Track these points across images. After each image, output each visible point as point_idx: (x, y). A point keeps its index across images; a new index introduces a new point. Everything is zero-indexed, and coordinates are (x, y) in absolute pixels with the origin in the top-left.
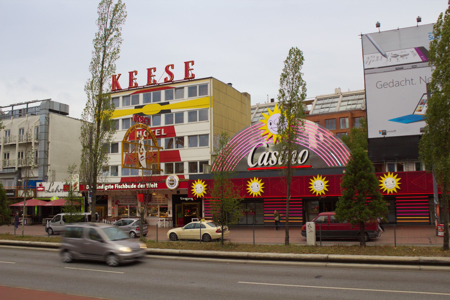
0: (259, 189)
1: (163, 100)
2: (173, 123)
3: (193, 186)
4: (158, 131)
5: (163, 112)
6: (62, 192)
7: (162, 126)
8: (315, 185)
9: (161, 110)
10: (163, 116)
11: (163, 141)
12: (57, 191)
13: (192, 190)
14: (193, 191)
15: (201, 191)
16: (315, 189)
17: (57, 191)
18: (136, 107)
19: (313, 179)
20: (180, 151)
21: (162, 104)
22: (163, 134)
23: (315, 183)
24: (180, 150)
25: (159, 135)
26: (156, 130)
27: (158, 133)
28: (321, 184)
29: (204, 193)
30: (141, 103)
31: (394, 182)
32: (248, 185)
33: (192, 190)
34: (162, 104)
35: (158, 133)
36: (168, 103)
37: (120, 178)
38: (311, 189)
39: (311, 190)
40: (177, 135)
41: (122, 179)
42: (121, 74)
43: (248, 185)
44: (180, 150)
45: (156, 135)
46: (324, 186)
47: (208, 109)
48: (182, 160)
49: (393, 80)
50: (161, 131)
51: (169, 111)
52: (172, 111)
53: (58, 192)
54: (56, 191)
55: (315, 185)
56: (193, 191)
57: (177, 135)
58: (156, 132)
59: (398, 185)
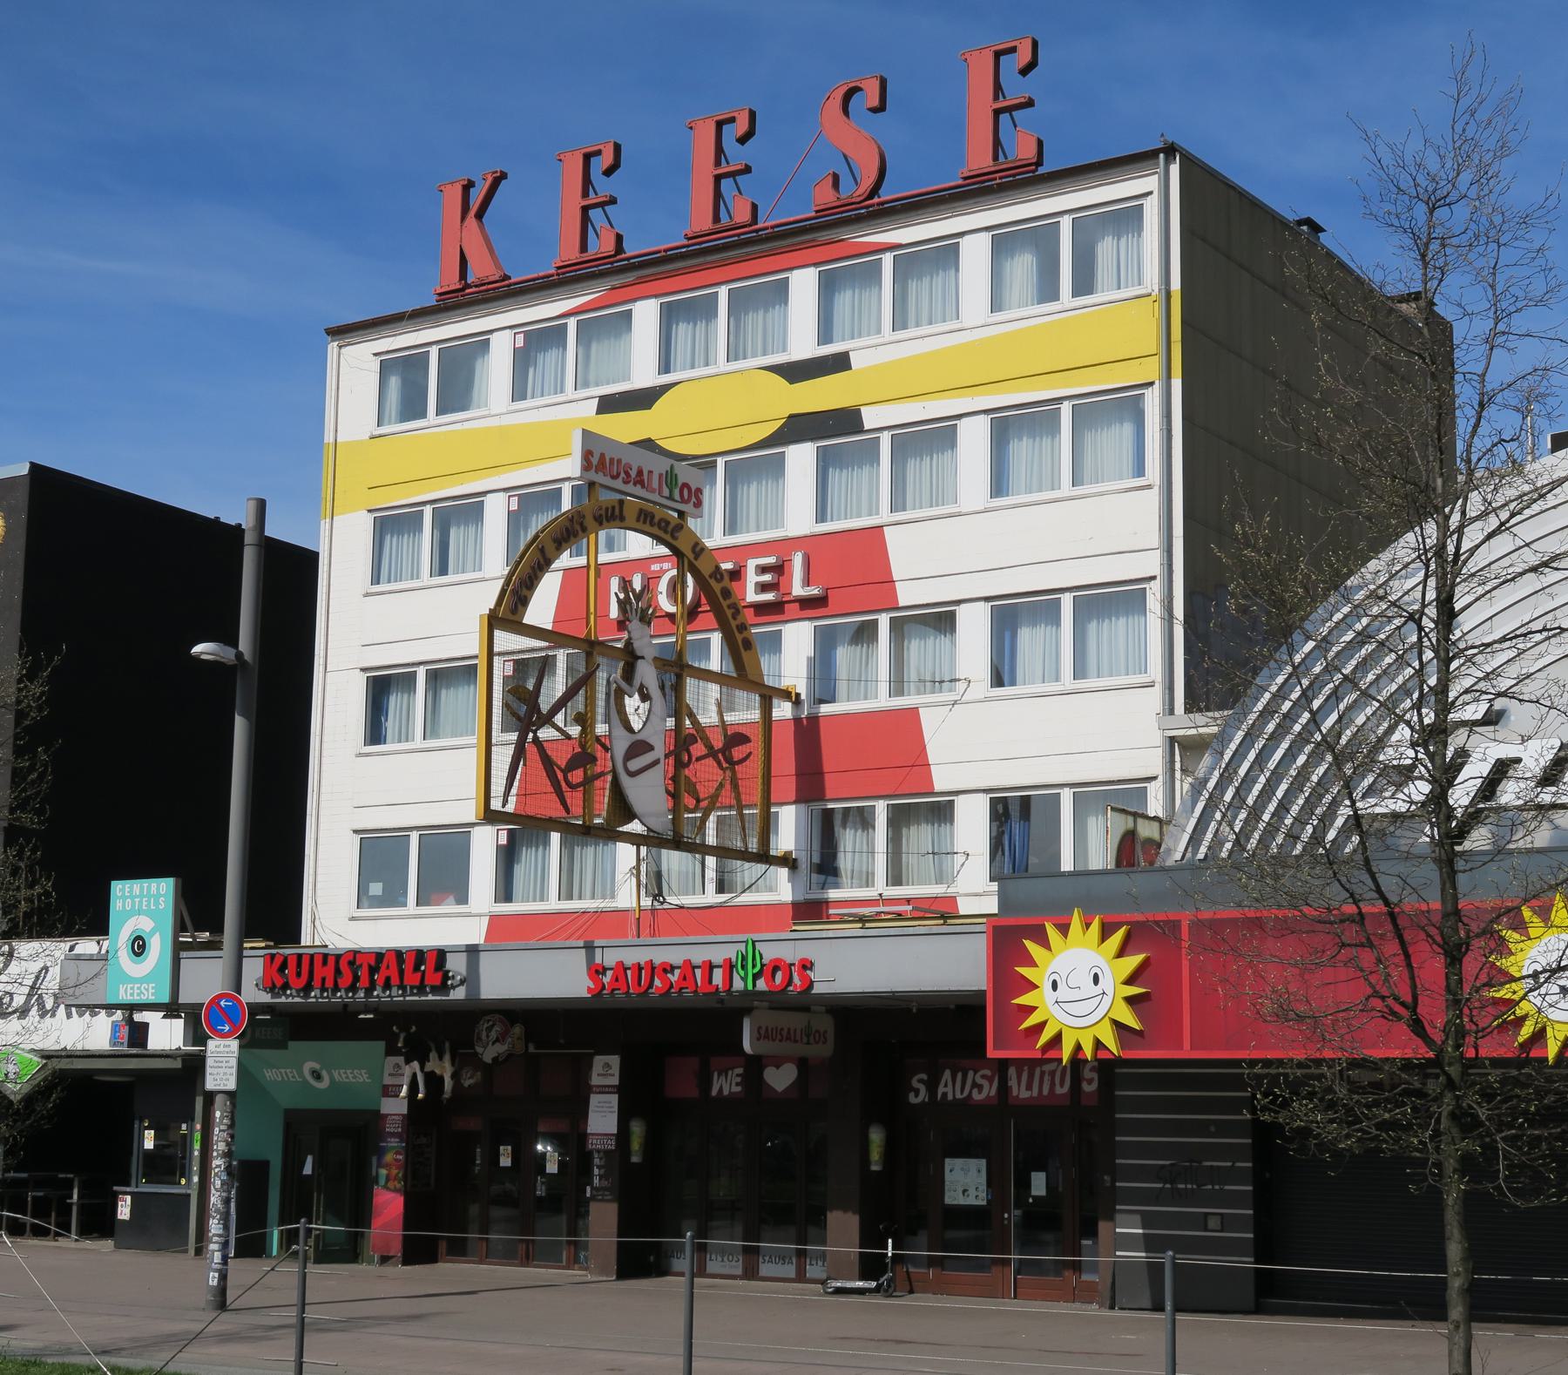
0: (1107, 1001)
1: (803, 345)
2: (873, 510)
3: (1031, 963)
4: (763, 570)
5: (798, 428)
6: (69, 1016)
7: (791, 534)
8: (1055, 986)
9: (791, 417)
10: (801, 458)
11: (798, 639)
12: (34, 1011)
13: (1024, 1000)
14: (1033, 1009)
15: (1091, 1005)
16: (1056, 1010)
17: (34, 1011)
18: (608, 405)
19: (1045, 943)
20: (924, 714)
21: (795, 372)
22: (798, 590)
23: (1053, 967)
24: (927, 705)
25: (769, 597)
26: (752, 564)
27: (763, 588)
28: (1096, 980)
29: (1118, 1026)
30: (644, 375)
31: (1107, 983)
32: (1024, 971)
33: (1024, 1000)
34: (795, 372)
35: (763, 588)
36: (840, 363)
37: (485, 921)
38: (1031, 1010)
39: (1031, 1021)
40: (907, 595)
41: (496, 921)
42: (503, 176)
43: (1024, 971)
44: (927, 705)
45: (752, 596)
46: (1110, 992)
47: (1148, 392)
48: (942, 780)
49: (1040, 143)
50: (779, 569)
51: (846, 420)
52: (870, 418)
53: (43, 1013)
54: (23, 1012)
55: (1055, 986)
56: (1033, 1009)
57: (907, 595)
58: (752, 578)
59: (1130, 1000)
